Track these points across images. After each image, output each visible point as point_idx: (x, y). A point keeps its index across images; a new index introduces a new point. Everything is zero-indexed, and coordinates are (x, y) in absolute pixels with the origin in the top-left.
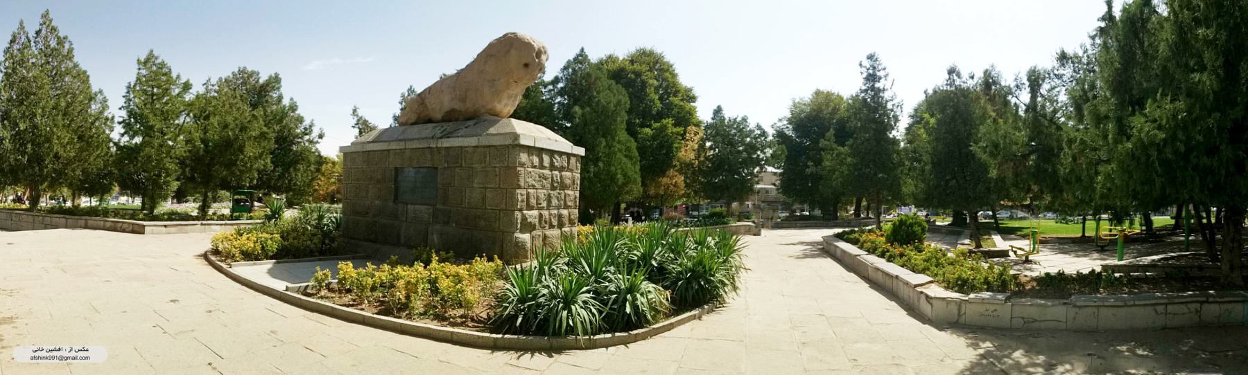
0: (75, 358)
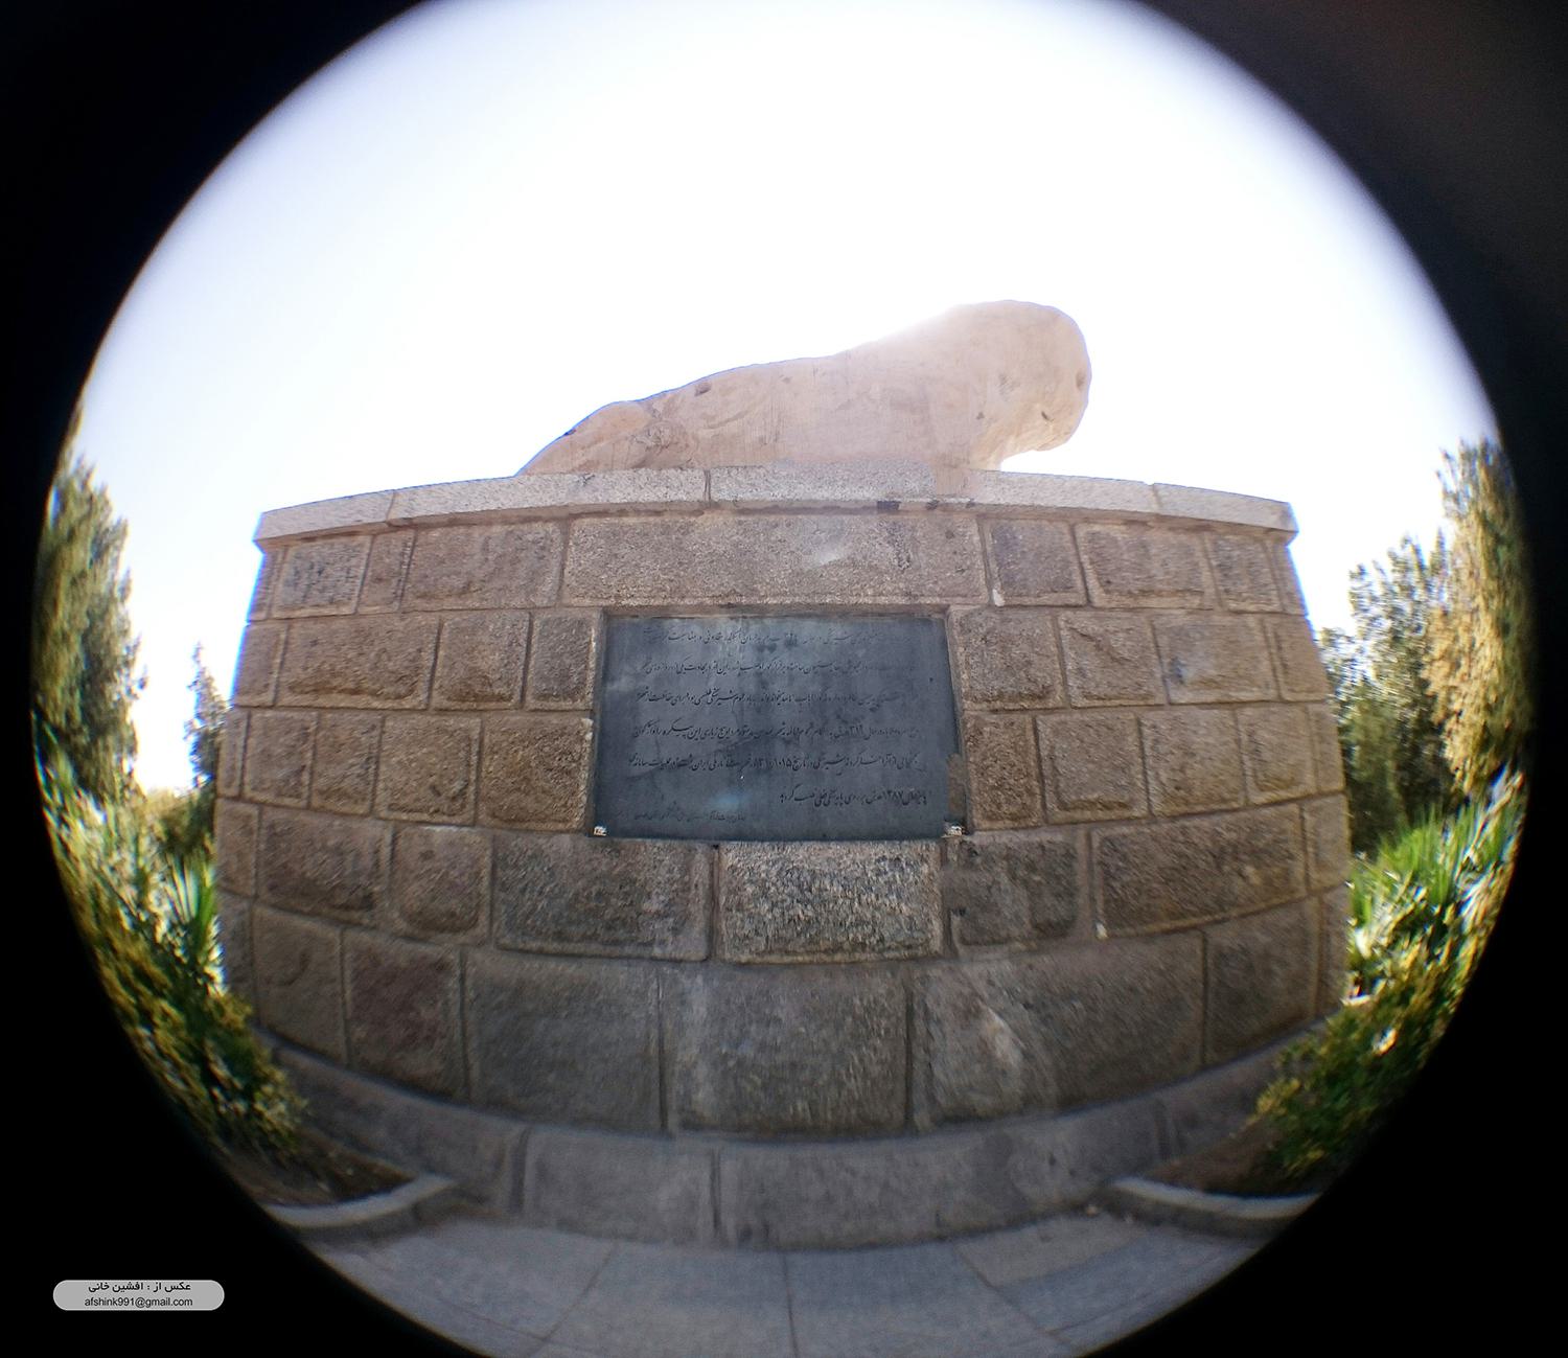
0: (164, 1303)
